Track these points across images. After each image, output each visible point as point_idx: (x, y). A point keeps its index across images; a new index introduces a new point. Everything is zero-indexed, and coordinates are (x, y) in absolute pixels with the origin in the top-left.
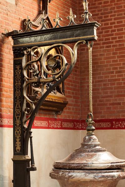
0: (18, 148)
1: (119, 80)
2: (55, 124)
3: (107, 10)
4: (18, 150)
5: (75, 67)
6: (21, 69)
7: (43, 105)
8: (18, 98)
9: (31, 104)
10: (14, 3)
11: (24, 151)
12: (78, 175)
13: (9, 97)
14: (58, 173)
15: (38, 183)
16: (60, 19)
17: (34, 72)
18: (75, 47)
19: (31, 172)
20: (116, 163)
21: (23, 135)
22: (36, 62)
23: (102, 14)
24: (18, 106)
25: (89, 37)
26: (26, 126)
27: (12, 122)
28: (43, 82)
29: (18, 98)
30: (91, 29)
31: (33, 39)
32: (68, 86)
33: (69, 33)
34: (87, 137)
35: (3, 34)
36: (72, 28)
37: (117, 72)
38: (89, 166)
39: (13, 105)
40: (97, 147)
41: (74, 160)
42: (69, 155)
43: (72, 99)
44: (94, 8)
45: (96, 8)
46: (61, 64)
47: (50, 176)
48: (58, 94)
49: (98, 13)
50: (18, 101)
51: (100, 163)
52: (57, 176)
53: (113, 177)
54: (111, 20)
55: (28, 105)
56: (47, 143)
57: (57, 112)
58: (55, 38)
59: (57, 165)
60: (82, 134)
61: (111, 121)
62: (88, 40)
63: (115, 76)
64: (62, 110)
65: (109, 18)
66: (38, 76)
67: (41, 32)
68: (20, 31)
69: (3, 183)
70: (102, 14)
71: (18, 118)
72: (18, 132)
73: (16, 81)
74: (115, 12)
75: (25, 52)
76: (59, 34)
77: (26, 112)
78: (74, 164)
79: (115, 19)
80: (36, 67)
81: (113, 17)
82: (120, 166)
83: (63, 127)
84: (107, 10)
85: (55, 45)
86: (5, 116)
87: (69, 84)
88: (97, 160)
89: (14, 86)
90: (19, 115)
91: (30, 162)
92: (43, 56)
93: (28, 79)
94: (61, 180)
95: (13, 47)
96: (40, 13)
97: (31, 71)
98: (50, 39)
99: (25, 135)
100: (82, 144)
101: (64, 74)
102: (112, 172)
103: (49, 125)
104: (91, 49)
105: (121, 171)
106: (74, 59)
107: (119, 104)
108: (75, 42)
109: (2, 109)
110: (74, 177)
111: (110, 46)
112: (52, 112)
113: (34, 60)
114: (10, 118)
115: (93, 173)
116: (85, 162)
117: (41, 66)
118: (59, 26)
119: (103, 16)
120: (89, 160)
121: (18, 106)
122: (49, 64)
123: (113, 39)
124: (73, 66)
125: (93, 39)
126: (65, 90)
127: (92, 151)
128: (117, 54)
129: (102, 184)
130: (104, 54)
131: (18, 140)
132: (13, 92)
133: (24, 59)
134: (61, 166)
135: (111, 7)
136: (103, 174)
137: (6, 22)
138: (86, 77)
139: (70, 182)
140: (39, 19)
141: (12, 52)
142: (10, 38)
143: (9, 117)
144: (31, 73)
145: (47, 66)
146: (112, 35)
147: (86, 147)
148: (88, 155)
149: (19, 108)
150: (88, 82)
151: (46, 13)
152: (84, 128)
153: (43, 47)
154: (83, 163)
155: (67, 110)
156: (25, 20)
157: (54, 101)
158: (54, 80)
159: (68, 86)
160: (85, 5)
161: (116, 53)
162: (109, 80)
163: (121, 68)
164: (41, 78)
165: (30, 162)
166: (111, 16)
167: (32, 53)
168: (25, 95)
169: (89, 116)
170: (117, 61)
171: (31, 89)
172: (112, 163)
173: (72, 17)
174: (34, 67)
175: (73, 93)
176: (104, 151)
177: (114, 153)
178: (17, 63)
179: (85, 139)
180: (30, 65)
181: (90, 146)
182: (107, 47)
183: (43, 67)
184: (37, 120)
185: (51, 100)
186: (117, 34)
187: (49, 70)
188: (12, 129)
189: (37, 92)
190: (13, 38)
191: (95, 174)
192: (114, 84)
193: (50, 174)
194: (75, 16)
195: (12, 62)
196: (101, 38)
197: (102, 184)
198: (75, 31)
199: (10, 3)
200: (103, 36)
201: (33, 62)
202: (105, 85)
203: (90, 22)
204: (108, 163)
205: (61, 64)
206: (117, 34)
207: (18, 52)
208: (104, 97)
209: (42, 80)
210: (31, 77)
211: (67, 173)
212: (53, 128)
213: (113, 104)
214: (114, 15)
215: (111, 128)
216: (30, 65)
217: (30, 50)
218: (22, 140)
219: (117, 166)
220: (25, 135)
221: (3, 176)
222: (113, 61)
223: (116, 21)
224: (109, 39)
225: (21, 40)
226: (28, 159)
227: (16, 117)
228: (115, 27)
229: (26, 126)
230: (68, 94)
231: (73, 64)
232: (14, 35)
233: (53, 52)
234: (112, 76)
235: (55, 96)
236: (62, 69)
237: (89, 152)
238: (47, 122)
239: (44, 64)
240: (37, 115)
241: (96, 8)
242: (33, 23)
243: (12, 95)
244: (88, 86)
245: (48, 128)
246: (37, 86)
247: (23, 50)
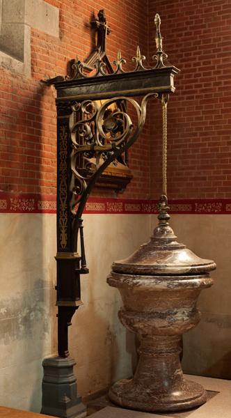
0: (64, 242)
1: (205, 145)
2: (112, 207)
3: (189, 44)
4: (64, 245)
5: (144, 131)
6: (68, 131)
7: (99, 181)
8: (63, 172)
9: (81, 181)
10: (57, 36)
11: (72, 248)
12: (146, 282)
13: (52, 171)
14: (118, 279)
15: (91, 289)
16: (122, 61)
17: (85, 137)
18: (143, 102)
19: (81, 275)
20: (199, 265)
21: (71, 224)
22: (90, 121)
23: (182, 51)
24: (63, 184)
25: (163, 87)
26: (74, 212)
27: (55, 205)
28: (98, 151)
29: (63, 172)
30: (166, 77)
31: (84, 89)
32: (133, 153)
33: (135, 82)
34: (159, 229)
35: (42, 81)
36: (139, 75)
37: (201, 134)
38: (161, 270)
39: (56, 181)
40: (173, 243)
41: (141, 261)
42: (134, 254)
43: (139, 171)
44: (171, 41)
45: (174, 41)
46: (123, 125)
47: (108, 282)
48: (120, 166)
49: (177, 49)
50: (63, 177)
51: (176, 266)
52: (118, 283)
53: (193, 285)
54: (195, 59)
55: (77, 182)
56: (100, 231)
57: (118, 191)
58: (115, 89)
59: (117, 268)
60: (152, 220)
61: (192, 202)
62: (161, 93)
63: (199, 139)
64: (125, 187)
65: (192, 56)
66: (91, 143)
67: (96, 80)
68: (66, 77)
69: (43, 290)
70: (182, 51)
71: (63, 200)
72: (63, 220)
73: (61, 149)
74: (200, 48)
75: (74, 109)
76: (121, 83)
77: (75, 193)
78: (140, 266)
79: (200, 59)
80: (89, 128)
81: (198, 56)
82: (204, 269)
83: (126, 210)
84: (189, 44)
85: (115, 98)
86: (45, 197)
87: (134, 151)
88: (171, 262)
89: (58, 156)
90: (65, 196)
91: (80, 262)
92: (98, 113)
93: (77, 147)
94: (123, 287)
95: (57, 101)
96: (94, 50)
97: (82, 135)
98: (109, 90)
99: (73, 224)
100: (152, 238)
101: (128, 140)
102: (193, 278)
103: (106, 208)
104: (166, 105)
105: (205, 277)
106: (142, 118)
107: (204, 179)
108: (144, 94)
109: (42, 187)
110: (140, 285)
111: (193, 97)
112: (110, 192)
113: (86, 119)
114: (52, 200)
115: (167, 279)
116: (155, 264)
117: (95, 128)
118: (121, 71)
119: (184, 53)
120: (162, 261)
121: (63, 184)
122: (107, 124)
123: (196, 86)
124: (141, 129)
125: (169, 91)
126: (129, 158)
127: (165, 249)
128: (202, 108)
129: (178, 295)
130: (184, 108)
131: (63, 231)
132: (56, 164)
133: (72, 118)
134: (122, 269)
135: (194, 41)
136: (180, 281)
137: (46, 64)
138: (159, 140)
139: (134, 292)
140: (92, 60)
141: (55, 108)
142: (52, 87)
143: (50, 199)
144: (81, 137)
145: (103, 127)
146: (196, 81)
147: (157, 244)
148: (159, 254)
149: (65, 187)
150: (161, 148)
151: (103, 50)
152: (155, 211)
153: (99, 101)
154: (152, 266)
155: (132, 187)
156: (73, 61)
157: (113, 175)
158: (113, 149)
159: (133, 153)
160: (159, 42)
161: (201, 108)
162: (190, 146)
163: (206, 128)
164: (96, 144)
165: (80, 262)
166: (195, 54)
167: (84, 110)
168: (73, 169)
169: (162, 200)
170: (201, 118)
171: (82, 159)
172: (192, 266)
173: (140, 59)
174: (86, 128)
175: (140, 163)
176: (182, 248)
177: (196, 251)
178: (62, 123)
179: (155, 231)
180: (80, 126)
181: (163, 241)
182: (188, 98)
183: (99, 129)
184: (89, 202)
185: (109, 174)
186: (202, 80)
187: (105, 132)
188: (56, 215)
189: (90, 164)
190: (56, 87)
191: (169, 282)
192: (197, 151)
193: (108, 279)
194: (145, 58)
195: (55, 121)
196: (181, 85)
197: (178, 295)
198: (144, 80)
199: (51, 36)
200: (183, 82)
201: (84, 122)
202: (184, 152)
203: (165, 67)
204: (187, 266)
205: (123, 125)
206: (202, 80)
207: (64, 108)
208: (183, 169)
209: (96, 148)
210: (81, 143)
211: (131, 279)
212: (112, 212)
213: (195, 179)
214: (199, 53)
215: (193, 212)
216: (80, 126)
217: (80, 104)
218: (69, 231)
219: (199, 269)
220: (73, 224)
221: (43, 281)
222: (197, 119)
223: (202, 61)
224: (191, 87)
225: (68, 90)
226: (77, 258)
227: (61, 199)
228: (200, 69)
229: (74, 212)
230: (132, 165)
231: (141, 125)
232: (58, 83)
233: (112, 107)
234: (195, 140)
235: (116, 168)
236: (124, 132)
237: (161, 249)
238: (103, 204)
239: (100, 123)
240: (90, 196)
241: (174, 41)
242: (84, 65)
243: (55, 168)
244: (161, 153)
245: (105, 212)
246: (90, 157)
247: (70, 106)
